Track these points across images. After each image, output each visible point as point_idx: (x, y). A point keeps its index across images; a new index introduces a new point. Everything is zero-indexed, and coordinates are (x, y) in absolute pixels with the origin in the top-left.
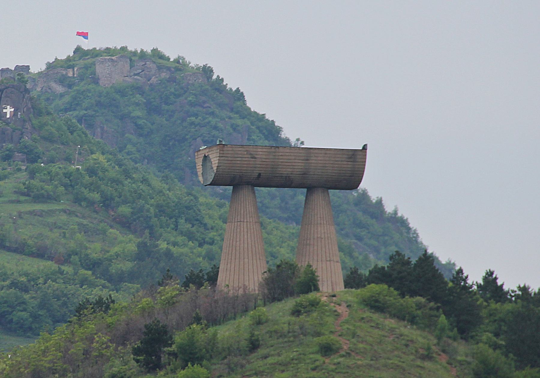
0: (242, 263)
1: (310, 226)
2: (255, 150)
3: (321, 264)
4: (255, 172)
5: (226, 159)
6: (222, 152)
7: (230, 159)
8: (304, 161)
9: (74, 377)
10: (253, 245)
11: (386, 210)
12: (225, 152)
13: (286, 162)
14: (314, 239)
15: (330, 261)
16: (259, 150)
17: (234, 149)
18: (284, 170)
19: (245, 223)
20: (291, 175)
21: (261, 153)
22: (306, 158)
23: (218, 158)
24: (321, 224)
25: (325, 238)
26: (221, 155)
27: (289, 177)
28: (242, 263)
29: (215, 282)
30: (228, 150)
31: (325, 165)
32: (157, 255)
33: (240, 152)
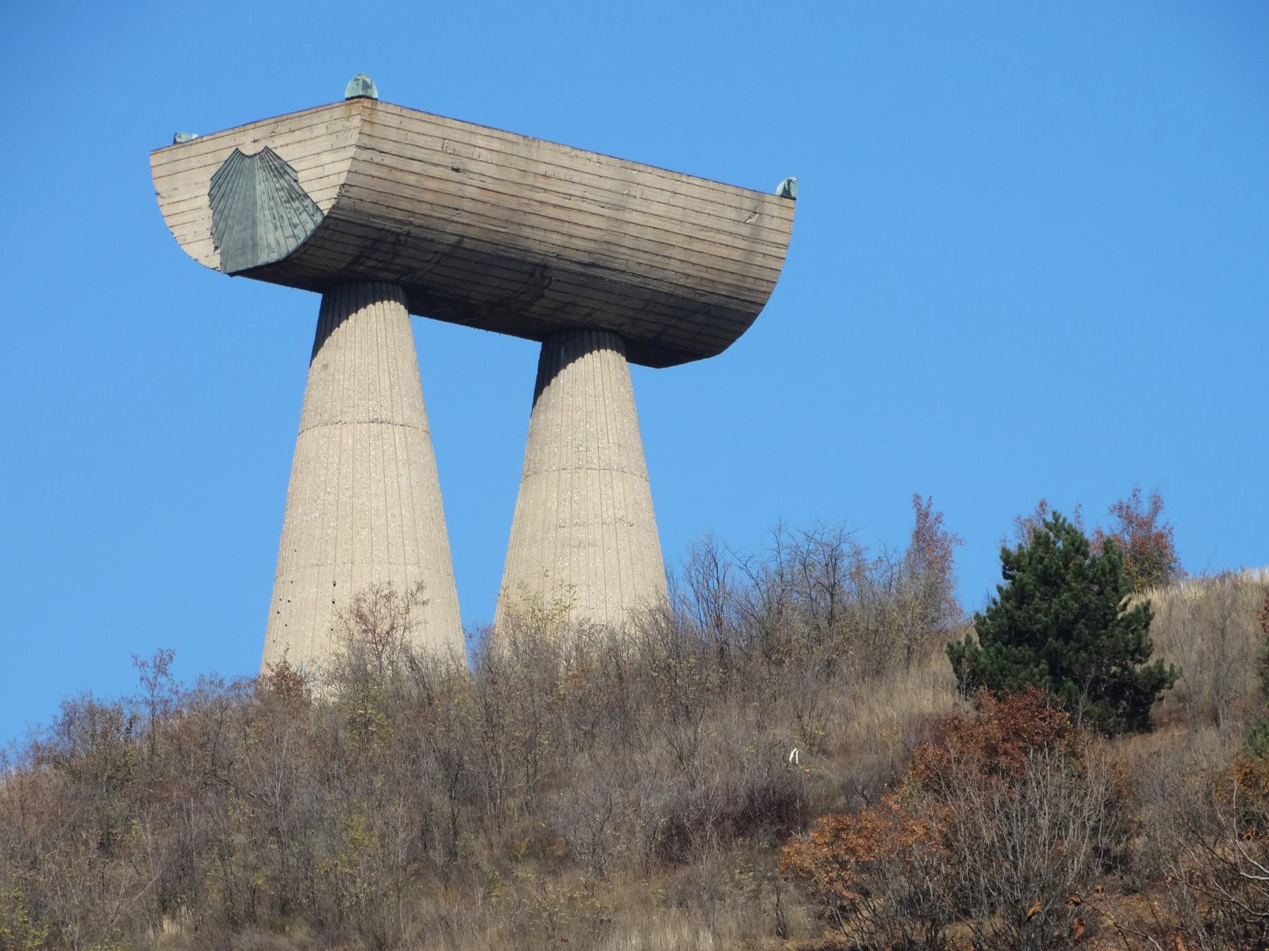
2: (466, 139)
5: (378, 158)
6: (367, 129)
7: (388, 160)
8: (605, 212)
9: (15, 949)
11: (392, 302)
13: (555, 206)
16: (481, 142)
17: (407, 124)
21: (485, 155)
22: (615, 199)
23: (352, 152)
26: (366, 141)
30: (385, 126)
32: (1087, 632)
33: (421, 140)
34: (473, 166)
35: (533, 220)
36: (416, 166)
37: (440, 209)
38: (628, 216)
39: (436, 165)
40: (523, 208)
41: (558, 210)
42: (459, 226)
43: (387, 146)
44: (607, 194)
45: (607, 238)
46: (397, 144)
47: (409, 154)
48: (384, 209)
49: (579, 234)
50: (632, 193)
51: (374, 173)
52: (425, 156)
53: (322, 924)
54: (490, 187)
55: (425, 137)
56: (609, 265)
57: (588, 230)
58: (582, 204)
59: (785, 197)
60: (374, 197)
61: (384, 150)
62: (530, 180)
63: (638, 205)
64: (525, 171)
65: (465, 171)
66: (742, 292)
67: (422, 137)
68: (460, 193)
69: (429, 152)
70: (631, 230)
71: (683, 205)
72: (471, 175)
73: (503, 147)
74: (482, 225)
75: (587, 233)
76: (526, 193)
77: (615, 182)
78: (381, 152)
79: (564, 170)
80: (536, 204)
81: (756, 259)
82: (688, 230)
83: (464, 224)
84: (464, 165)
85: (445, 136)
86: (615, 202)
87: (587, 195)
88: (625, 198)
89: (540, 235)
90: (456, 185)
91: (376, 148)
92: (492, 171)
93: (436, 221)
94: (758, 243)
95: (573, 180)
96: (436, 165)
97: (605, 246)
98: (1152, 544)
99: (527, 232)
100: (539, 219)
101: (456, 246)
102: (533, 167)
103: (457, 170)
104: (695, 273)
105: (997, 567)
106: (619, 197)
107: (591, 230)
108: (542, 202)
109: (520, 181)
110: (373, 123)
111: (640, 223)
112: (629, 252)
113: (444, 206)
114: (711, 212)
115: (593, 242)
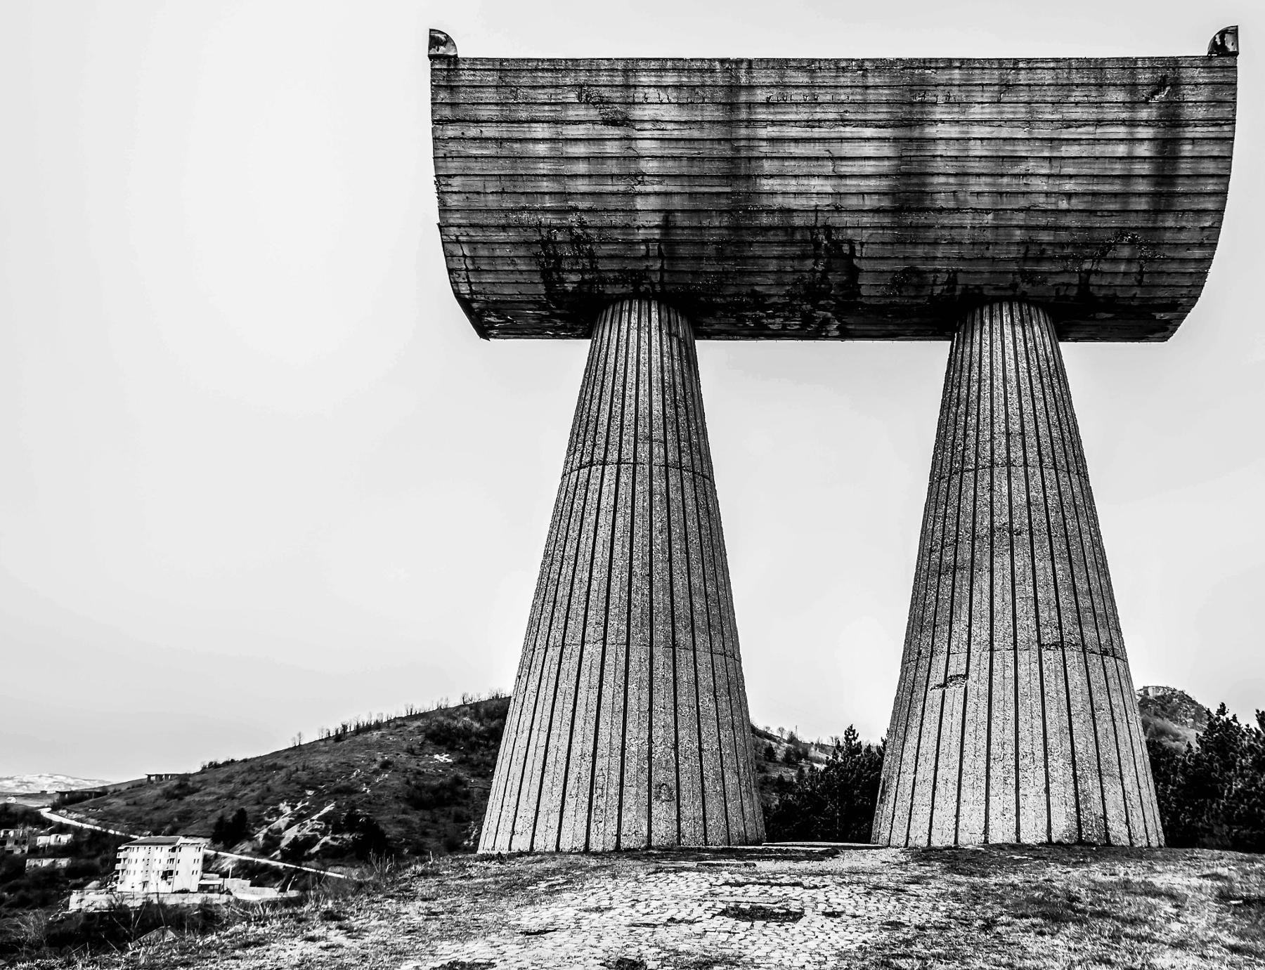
0: (570, 665)
1: (956, 479)
3: (768, 81)
4: (640, 203)
10: (637, 570)
12: (461, 97)
14: (974, 538)
15: (1060, 644)
18: (792, 185)
19: (610, 470)
20: (835, 220)
22: (901, 112)
24: (1009, 463)
25: (1099, 104)
26: (447, 112)
27: (828, 229)
28: (570, 665)
29: (321, 761)
31: (1007, 150)
55: (546, 90)
58: (842, 129)
80: (764, 144)
81: (972, 110)
95: (819, 101)
104: (1080, 189)
114: (1078, 99)
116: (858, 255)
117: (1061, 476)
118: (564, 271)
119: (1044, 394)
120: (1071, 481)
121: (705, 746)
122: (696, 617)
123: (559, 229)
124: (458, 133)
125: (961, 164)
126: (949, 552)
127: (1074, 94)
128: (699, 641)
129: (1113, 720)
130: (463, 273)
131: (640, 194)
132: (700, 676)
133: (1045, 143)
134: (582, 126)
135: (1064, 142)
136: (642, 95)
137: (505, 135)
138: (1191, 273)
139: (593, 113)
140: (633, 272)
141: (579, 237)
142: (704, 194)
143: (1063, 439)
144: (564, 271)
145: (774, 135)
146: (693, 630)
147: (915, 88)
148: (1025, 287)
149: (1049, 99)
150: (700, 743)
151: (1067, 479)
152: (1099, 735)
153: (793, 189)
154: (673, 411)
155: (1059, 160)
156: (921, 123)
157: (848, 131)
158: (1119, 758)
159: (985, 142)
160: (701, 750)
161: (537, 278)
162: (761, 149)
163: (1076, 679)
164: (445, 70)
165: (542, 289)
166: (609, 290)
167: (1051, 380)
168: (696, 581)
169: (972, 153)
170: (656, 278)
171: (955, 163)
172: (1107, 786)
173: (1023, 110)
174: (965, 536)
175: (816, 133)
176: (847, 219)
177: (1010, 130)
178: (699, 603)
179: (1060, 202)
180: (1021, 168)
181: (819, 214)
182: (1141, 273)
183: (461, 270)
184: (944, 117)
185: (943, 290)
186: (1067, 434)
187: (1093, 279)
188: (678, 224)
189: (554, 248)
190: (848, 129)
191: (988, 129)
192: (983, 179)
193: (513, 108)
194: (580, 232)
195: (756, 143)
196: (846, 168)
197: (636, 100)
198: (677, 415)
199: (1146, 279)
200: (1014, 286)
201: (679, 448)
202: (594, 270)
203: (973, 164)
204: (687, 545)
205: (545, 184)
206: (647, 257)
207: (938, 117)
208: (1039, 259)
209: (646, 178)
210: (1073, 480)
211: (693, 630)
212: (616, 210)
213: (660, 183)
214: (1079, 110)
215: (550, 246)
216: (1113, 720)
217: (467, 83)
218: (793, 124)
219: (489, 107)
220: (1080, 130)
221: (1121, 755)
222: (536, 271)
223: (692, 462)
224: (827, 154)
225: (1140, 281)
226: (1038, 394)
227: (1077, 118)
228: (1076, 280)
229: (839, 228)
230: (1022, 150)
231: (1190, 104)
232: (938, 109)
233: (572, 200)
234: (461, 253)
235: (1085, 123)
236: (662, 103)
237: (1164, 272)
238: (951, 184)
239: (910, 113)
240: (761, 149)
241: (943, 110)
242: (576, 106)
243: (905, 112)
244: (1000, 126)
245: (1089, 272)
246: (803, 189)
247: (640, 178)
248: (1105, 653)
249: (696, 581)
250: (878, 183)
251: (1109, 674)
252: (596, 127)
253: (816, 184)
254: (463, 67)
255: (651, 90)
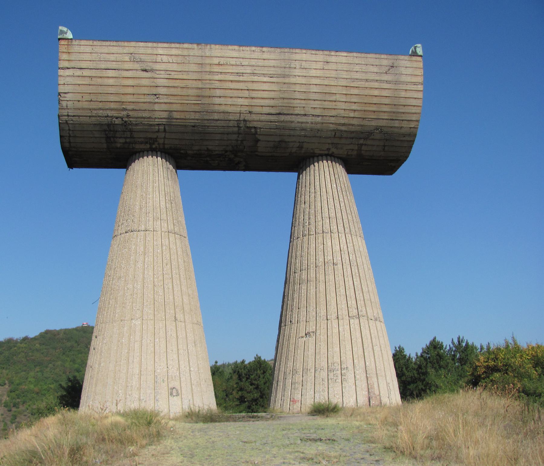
5: (78, 73)
7: (86, 73)
21: (165, 58)
22: (279, 71)
31: (327, 90)
34: (157, 67)
35: (218, 93)
36: (111, 73)
37: (142, 97)
38: (293, 80)
39: (127, 70)
40: (208, 86)
41: (234, 84)
42: (163, 105)
43: (83, 65)
44: (273, 69)
45: (282, 96)
46: (92, 62)
47: (103, 66)
48: (342, 112)
49: (259, 96)
50: (292, 66)
51: (79, 82)
52: (117, 66)
53: (289, 438)
54: (176, 77)
55: (115, 55)
56: (291, 112)
57: (264, 92)
58: (253, 77)
59: (414, 56)
60: (87, 97)
61: (83, 67)
62: (208, 69)
63: (298, 72)
64: (202, 64)
65: (152, 70)
66: (399, 115)
67: (112, 55)
68: (154, 84)
69: (120, 63)
70: (298, 88)
71: (335, 68)
72: (157, 72)
73: (237, 55)
74: (180, 102)
75: (265, 95)
76: (208, 77)
77: (277, 62)
78: (81, 69)
79: (235, 59)
80: (217, 82)
81: (312, 72)
82: (344, 83)
83: (166, 103)
84: (150, 67)
85: (132, 52)
86: (279, 72)
87: (255, 72)
88: (287, 70)
89: (230, 101)
90: (147, 80)
91: (76, 67)
92: (175, 67)
93: (142, 104)
94: (399, 84)
95: (243, 64)
96: (127, 70)
97: (281, 101)
98: (471, 387)
99: (217, 101)
100: (222, 91)
101: (170, 118)
102: (208, 61)
103: (146, 71)
104: (359, 108)
105: (426, 342)
106: (283, 69)
107: (267, 92)
108: (221, 81)
109: (200, 70)
110: (69, 53)
111: (303, 83)
112: (303, 102)
113: (144, 94)
114: (357, 70)
115: (272, 100)
116: (258, 133)
117: (353, 237)
118: (117, 137)
119: (344, 199)
120: (358, 240)
121: (192, 369)
122: (184, 306)
123: (117, 118)
124: (71, 74)
125: (306, 95)
126: (304, 273)
127: (355, 67)
128: (186, 317)
129: (381, 350)
130: (67, 138)
131: (158, 103)
132: (188, 335)
133: (344, 88)
134: (130, 72)
135: (352, 88)
136: (160, 59)
137: (94, 75)
138: (405, 147)
139: (137, 66)
140: (151, 138)
141: (126, 122)
142: (187, 104)
143: (353, 220)
144: (117, 137)
145: (222, 79)
146: (184, 312)
147: (286, 61)
148: (333, 150)
149: (345, 69)
150: (190, 368)
151: (356, 239)
152: (376, 358)
153: (230, 103)
154: (170, 205)
155: (350, 95)
156: (288, 76)
157: (256, 78)
158: (384, 368)
159: (318, 86)
160: (190, 371)
161: (103, 141)
162: (216, 85)
163: (366, 332)
164: (66, 45)
165: (105, 146)
166: (138, 146)
167: (346, 193)
168: (184, 289)
169: (312, 91)
170: (161, 141)
171: (304, 95)
172: (380, 380)
173: (334, 73)
174: (312, 266)
175: (241, 78)
176: (254, 117)
177: (328, 81)
178: (186, 300)
179: (350, 114)
180: (333, 98)
181: (241, 115)
182: (384, 146)
183: (67, 136)
184: (299, 74)
185: (297, 150)
186: (354, 218)
187: (364, 148)
188: (175, 117)
189: (114, 127)
190: (256, 77)
191: (319, 80)
192: (316, 102)
193: (98, 62)
194: (127, 119)
195: (213, 82)
196: (254, 94)
197: (157, 61)
198: (172, 207)
199: (386, 148)
200: (328, 149)
201: (174, 223)
202: (132, 137)
203: (312, 95)
204: (179, 270)
205: (112, 97)
206: (158, 131)
207: (297, 74)
208: (341, 138)
209: (160, 96)
210: (358, 239)
211: (184, 312)
212: (145, 110)
213: (167, 98)
214: (358, 74)
215: (112, 126)
216: (381, 350)
217: (77, 51)
218: (231, 74)
219: (87, 62)
220: (358, 83)
221: (385, 366)
222: (103, 137)
223: (179, 230)
224: (246, 88)
225: (384, 149)
226: (341, 199)
227: (357, 78)
228: (356, 148)
229: (250, 121)
230: (333, 90)
231: (404, 75)
232: (297, 71)
233: (124, 105)
234: (67, 128)
235: (361, 80)
236: (169, 63)
237: (394, 146)
238: (303, 104)
239: (284, 71)
240: (216, 85)
241: (299, 71)
242: (128, 63)
243: (282, 71)
244: (324, 79)
245: (362, 145)
246: (234, 103)
247: (157, 96)
248: (376, 320)
249: (184, 289)
250: (269, 102)
251: (378, 329)
252: (138, 72)
253: (241, 101)
254: (75, 44)
255: (164, 56)
